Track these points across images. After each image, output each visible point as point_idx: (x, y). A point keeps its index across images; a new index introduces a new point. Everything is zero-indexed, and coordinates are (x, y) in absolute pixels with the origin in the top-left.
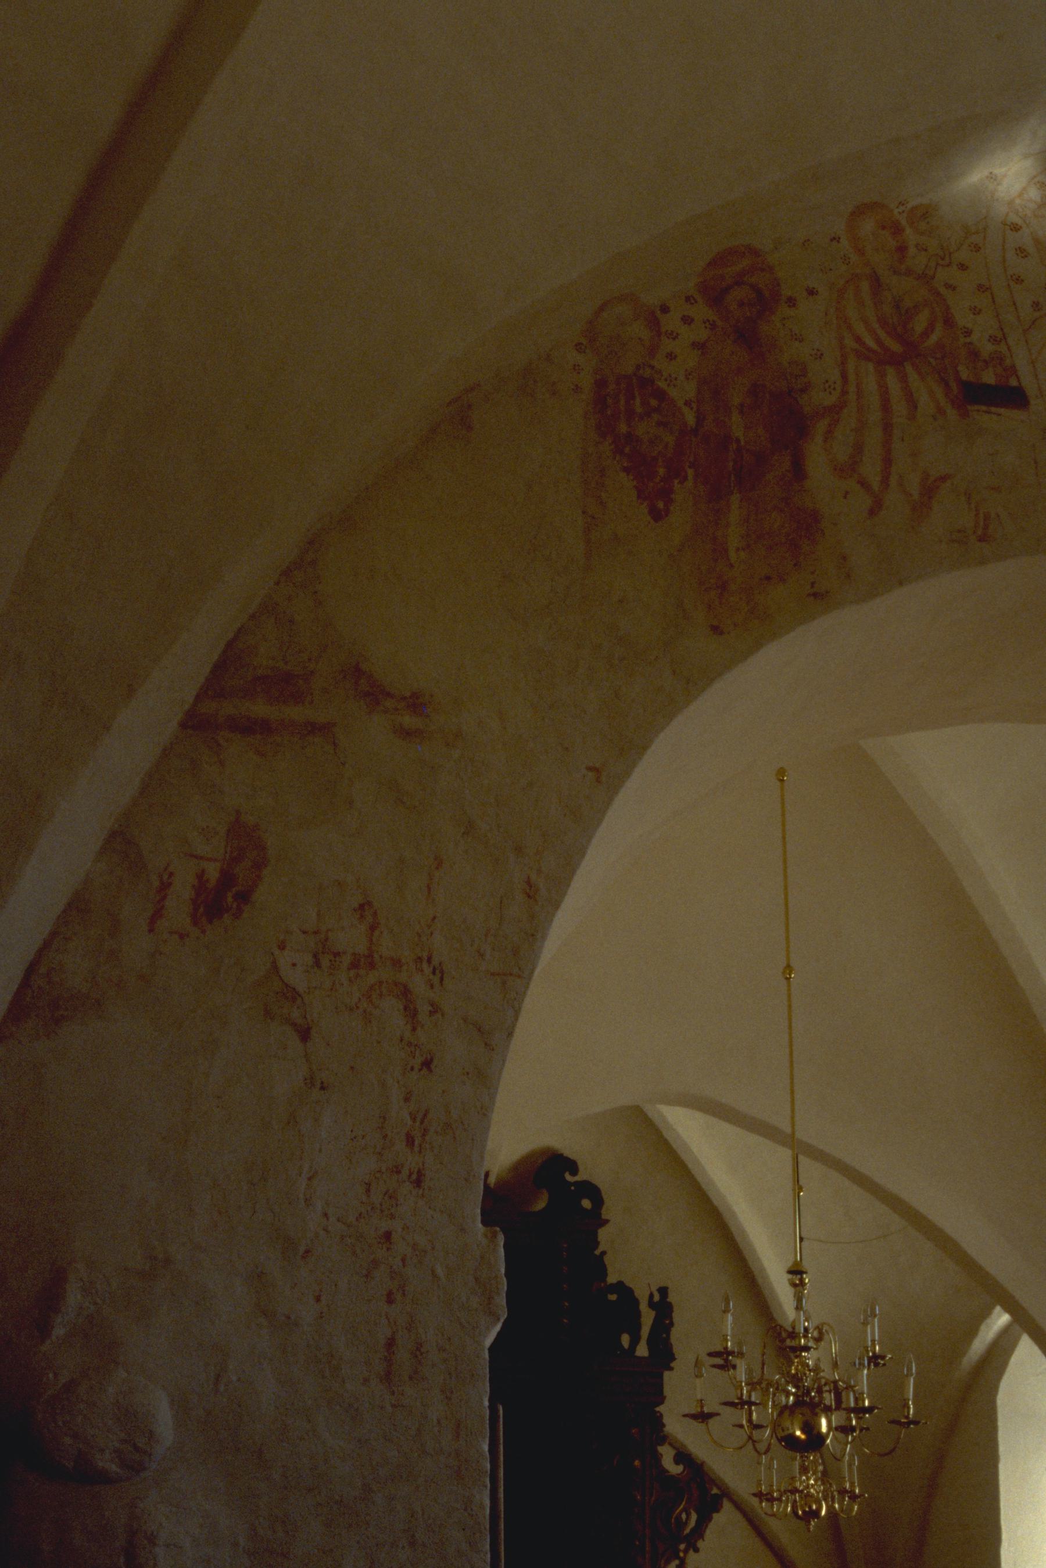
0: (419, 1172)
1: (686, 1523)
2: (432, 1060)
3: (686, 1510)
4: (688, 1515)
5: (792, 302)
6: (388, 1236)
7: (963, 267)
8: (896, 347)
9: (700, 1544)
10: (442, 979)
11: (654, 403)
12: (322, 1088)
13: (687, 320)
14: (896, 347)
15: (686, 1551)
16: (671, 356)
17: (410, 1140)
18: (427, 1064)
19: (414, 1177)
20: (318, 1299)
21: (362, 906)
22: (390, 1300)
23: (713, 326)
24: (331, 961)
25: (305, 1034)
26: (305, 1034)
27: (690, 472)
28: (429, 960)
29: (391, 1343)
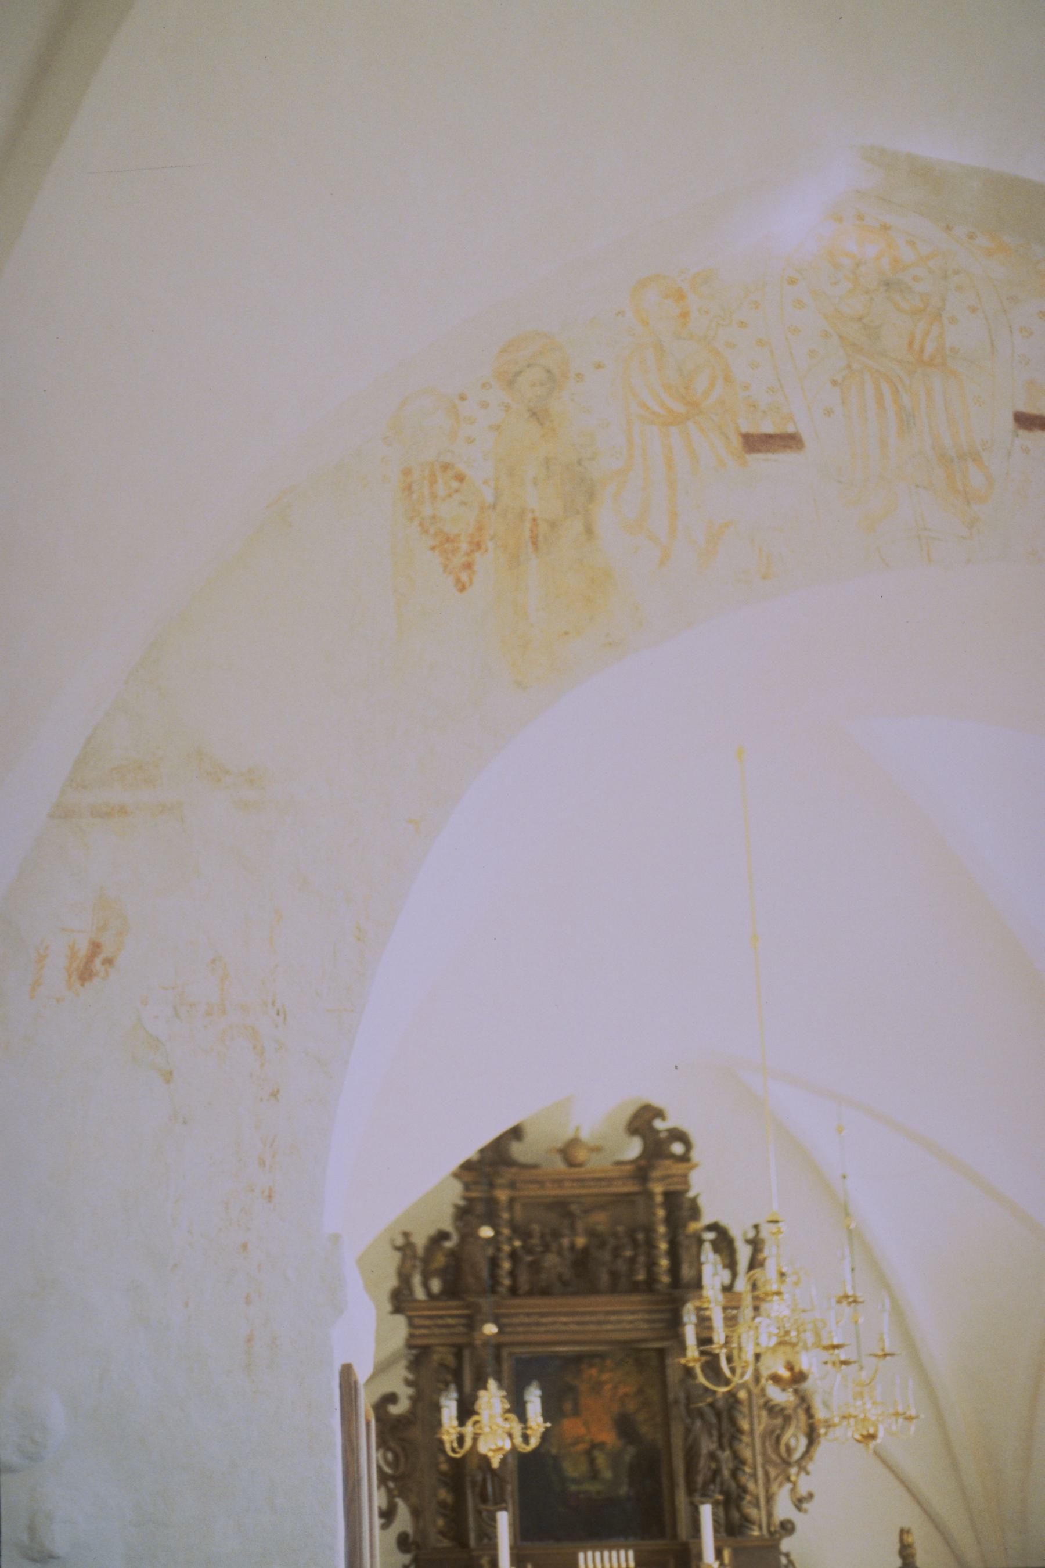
0: (270, 1189)
1: (795, 1449)
2: (278, 1091)
3: (795, 1436)
4: (797, 1440)
5: (579, 376)
6: (245, 1246)
7: (742, 324)
8: (680, 408)
9: (810, 1467)
10: (285, 1018)
11: (455, 484)
12: (185, 1123)
13: (484, 405)
14: (680, 408)
15: (798, 1474)
16: (470, 440)
17: (262, 1163)
18: (274, 1095)
19: (266, 1193)
20: (187, 1305)
21: (213, 961)
22: (248, 1301)
23: (508, 407)
24: (188, 1011)
25: (168, 1076)
26: (168, 1076)
27: (490, 545)
28: (273, 1004)
29: (249, 1340)
